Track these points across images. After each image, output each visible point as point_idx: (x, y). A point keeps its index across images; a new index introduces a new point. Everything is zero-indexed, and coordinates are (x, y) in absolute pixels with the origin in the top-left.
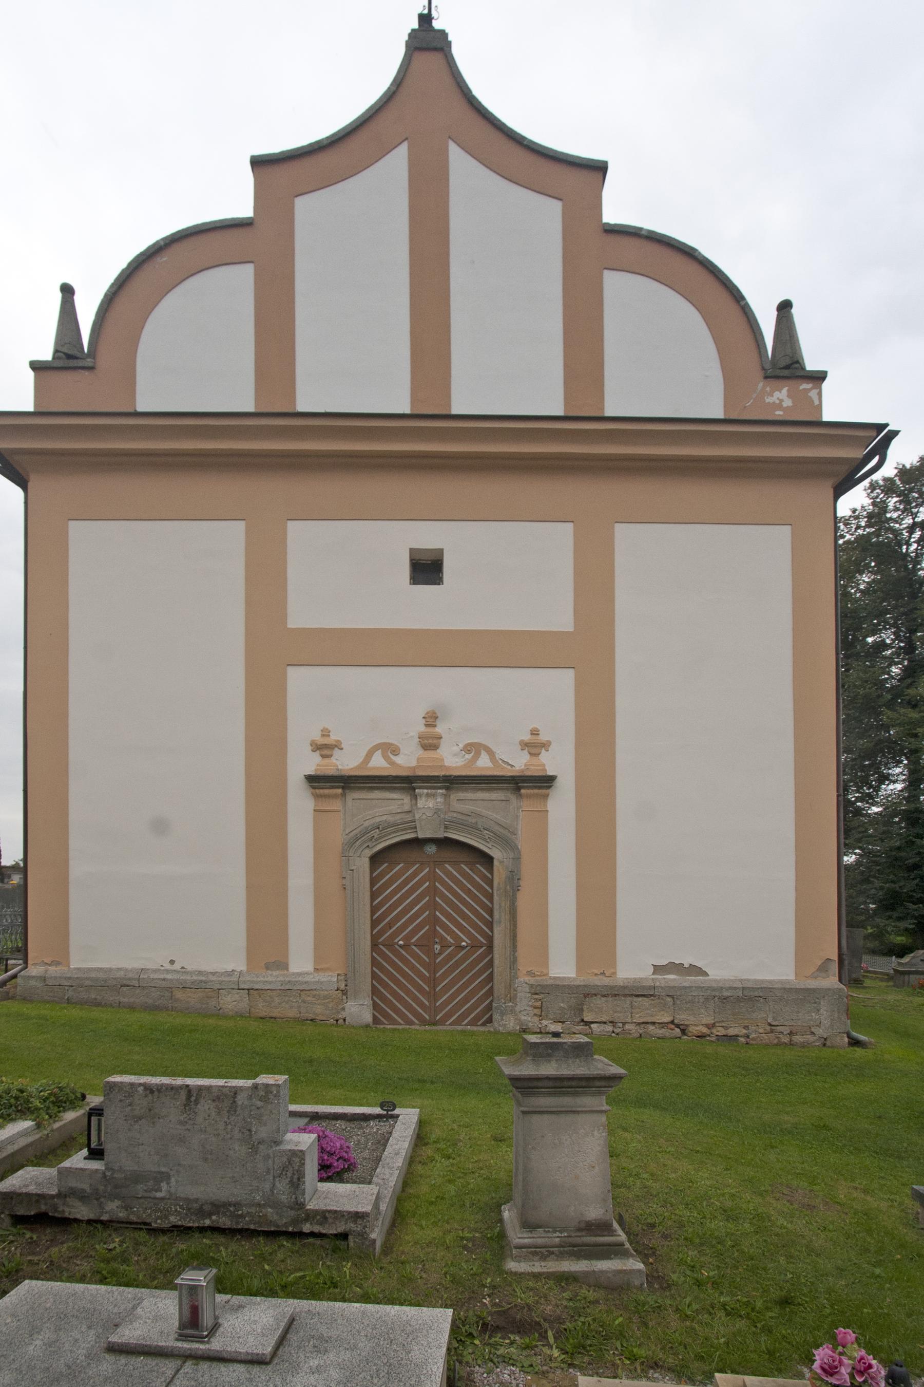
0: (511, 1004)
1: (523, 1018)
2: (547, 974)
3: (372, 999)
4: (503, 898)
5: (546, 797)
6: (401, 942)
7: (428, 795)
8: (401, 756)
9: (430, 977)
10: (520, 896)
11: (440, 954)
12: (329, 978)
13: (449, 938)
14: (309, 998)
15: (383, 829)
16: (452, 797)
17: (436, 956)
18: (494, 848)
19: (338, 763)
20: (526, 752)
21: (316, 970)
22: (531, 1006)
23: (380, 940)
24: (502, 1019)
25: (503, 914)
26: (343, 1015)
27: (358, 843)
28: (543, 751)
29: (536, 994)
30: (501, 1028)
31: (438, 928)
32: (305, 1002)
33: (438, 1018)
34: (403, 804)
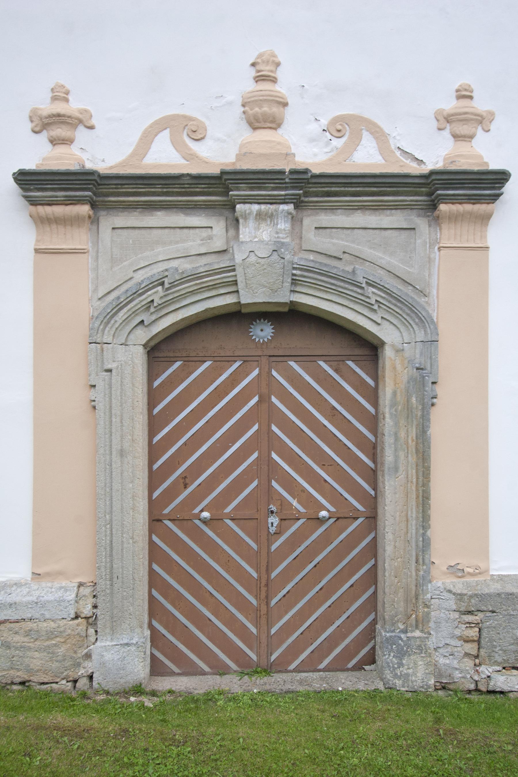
0: (417, 633)
1: (442, 661)
2: (487, 571)
3: (151, 626)
4: (402, 422)
5: (486, 218)
6: (206, 514)
7: (260, 217)
8: (208, 142)
9: (260, 577)
10: (435, 414)
11: (278, 533)
12: (60, 593)
13: (295, 503)
14: (17, 638)
15: (173, 285)
16: (307, 221)
17: (271, 538)
18: (385, 324)
19: (84, 156)
20: (446, 133)
21: (36, 575)
22: (460, 638)
23: (166, 511)
24: (400, 665)
25: (402, 455)
26: (89, 667)
27: (121, 314)
28: (480, 131)
29: (470, 613)
30: (398, 683)
31: (274, 484)
32: (8, 647)
33: (273, 658)
34: (210, 238)
